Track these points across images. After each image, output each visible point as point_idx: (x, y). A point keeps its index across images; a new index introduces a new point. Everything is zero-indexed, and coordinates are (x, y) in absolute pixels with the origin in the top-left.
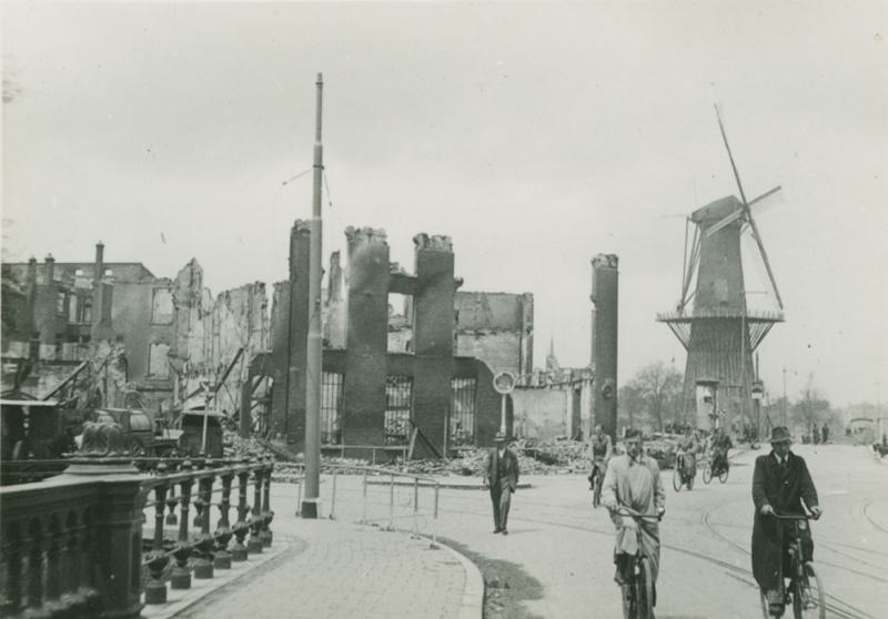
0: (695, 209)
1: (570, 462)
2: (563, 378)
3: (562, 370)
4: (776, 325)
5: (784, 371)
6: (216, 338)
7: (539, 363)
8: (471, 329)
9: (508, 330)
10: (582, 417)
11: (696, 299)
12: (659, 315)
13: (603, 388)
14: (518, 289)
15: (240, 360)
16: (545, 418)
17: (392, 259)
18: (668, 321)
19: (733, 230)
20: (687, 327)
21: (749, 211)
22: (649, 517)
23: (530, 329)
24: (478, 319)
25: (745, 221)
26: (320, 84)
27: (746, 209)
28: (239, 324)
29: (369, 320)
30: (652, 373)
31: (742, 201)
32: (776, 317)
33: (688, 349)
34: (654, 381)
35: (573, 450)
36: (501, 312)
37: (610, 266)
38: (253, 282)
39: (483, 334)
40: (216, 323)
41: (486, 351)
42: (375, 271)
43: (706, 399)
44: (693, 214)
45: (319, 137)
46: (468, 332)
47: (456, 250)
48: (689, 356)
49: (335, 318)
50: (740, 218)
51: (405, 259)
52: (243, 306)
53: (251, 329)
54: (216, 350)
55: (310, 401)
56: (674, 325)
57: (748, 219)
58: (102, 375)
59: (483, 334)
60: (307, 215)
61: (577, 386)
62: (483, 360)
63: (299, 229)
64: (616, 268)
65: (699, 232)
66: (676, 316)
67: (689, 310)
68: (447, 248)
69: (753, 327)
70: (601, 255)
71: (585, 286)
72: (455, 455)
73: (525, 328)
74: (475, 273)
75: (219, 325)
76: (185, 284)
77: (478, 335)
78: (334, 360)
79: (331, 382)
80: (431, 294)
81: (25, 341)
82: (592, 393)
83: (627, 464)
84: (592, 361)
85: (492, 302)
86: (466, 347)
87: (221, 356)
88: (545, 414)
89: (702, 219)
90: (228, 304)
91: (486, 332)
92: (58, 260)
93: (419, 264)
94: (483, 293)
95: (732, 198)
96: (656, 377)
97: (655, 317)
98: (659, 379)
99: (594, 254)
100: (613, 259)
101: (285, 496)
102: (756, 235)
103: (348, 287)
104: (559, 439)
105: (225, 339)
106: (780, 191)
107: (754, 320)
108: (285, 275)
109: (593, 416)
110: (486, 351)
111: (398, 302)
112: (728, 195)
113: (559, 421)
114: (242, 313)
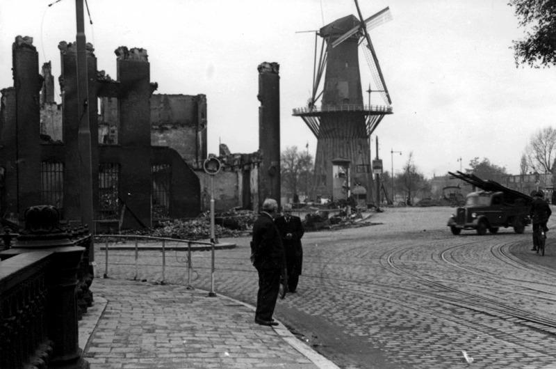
0: (322, 26)
1: (247, 227)
2: (234, 161)
3: (234, 155)
4: (386, 116)
5: (392, 152)
7: (213, 149)
10: (252, 192)
11: (323, 98)
12: (294, 110)
14: (194, 92)
16: (221, 193)
17: (99, 69)
18: (303, 115)
19: (353, 43)
21: (365, 28)
25: (362, 35)
27: (363, 25)
30: (289, 156)
31: (359, 19)
33: (318, 137)
34: (290, 162)
35: (249, 217)
37: (273, 72)
39: (167, 129)
41: (169, 141)
43: (340, 175)
44: (321, 30)
47: (150, 59)
48: (319, 143)
50: (357, 33)
51: (108, 66)
56: (306, 118)
57: (364, 33)
59: (167, 129)
60: (71, 38)
61: (246, 167)
62: (175, 149)
63: (20, 43)
67: (319, 105)
70: (265, 63)
72: (157, 226)
73: (200, 123)
79: (53, 169)
85: (173, 101)
86: (159, 139)
88: (221, 190)
89: (327, 33)
91: (169, 127)
92: (60, 93)
94: (165, 95)
95: (351, 17)
96: (292, 160)
97: (292, 113)
98: (294, 160)
100: (275, 66)
102: (370, 46)
104: (237, 210)
106: (388, 11)
110: (169, 141)
112: (349, 14)
113: (232, 195)
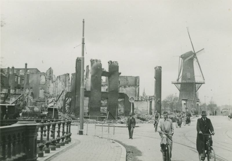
0: (181, 54)
1: (149, 120)
2: (147, 98)
3: (147, 96)
4: (203, 84)
5: (205, 97)
6: (57, 88)
7: (141, 94)
8: (123, 86)
9: (133, 86)
10: (152, 109)
11: (182, 78)
12: (172, 82)
13: (158, 101)
14: (135, 75)
15: (63, 94)
16: (142, 109)
17: (103, 67)
18: (175, 84)
19: (192, 60)
20: (180, 85)
21: (196, 55)
22: (170, 134)
23: (138, 86)
24: (125, 83)
25: (195, 57)
26: (84, 22)
27: (195, 54)
28: (63, 84)
29: (96, 83)
30: (170, 97)
31: (194, 52)
32: (203, 82)
33: (180, 91)
34: (171, 99)
35: (150, 117)
36: (131, 81)
37: (159, 69)
38: (66, 73)
39: (126, 87)
40: (56, 84)
41: (127, 91)
42: (98, 71)
43: (184, 104)
44: (181, 56)
45: (83, 36)
46: (122, 86)
47: (119, 65)
48: (180, 93)
49: (87, 83)
50: (193, 57)
51: (106, 67)
52: (63, 79)
53: (66, 86)
54: (56, 91)
55: (81, 104)
56: (176, 85)
57: (195, 57)
58: (27, 97)
59: (126, 87)
60: (80, 56)
61: (151, 101)
62: (126, 94)
63: (78, 59)
64: (161, 70)
65: (183, 60)
66: (177, 82)
67: (180, 81)
68: (117, 64)
69: (197, 85)
70: (157, 66)
71: (153, 74)
72: (119, 118)
73: (137, 85)
74: (124, 71)
75: (57, 85)
76: (48, 74)
77: (125, 87)
78: (87, 94)
79: (86, 99)
80: (113, 77)
81: (7, 89)
82: (155, 102)
83: (164, 121)
84: (155, 94)
85: (129, 79)
86: (122, 90)
87: (58, 93)
88: (142, 108)
89: (183, 57)
90: (60, 79)
91: (127, 86)
92: (15, 68)
93: (110, 69)
94: (126, 76)
95: (191, 52)
96: (172, 98)
97: (171, 82)
98: (172, 99)
99: (155, 66)
100: (160, 67)
101: (74, 129)
102: (197, 61)
103: (91, 75)
104: (146, 114)
105: (59, 88)
106: (204, 50)
107: (197, 83)
108: (74, 72)
109: (155, 108)
110: (127, 91)
111: (104, 79)
112: (190, 51)
113: (146, 110)
114: (63, 81)
